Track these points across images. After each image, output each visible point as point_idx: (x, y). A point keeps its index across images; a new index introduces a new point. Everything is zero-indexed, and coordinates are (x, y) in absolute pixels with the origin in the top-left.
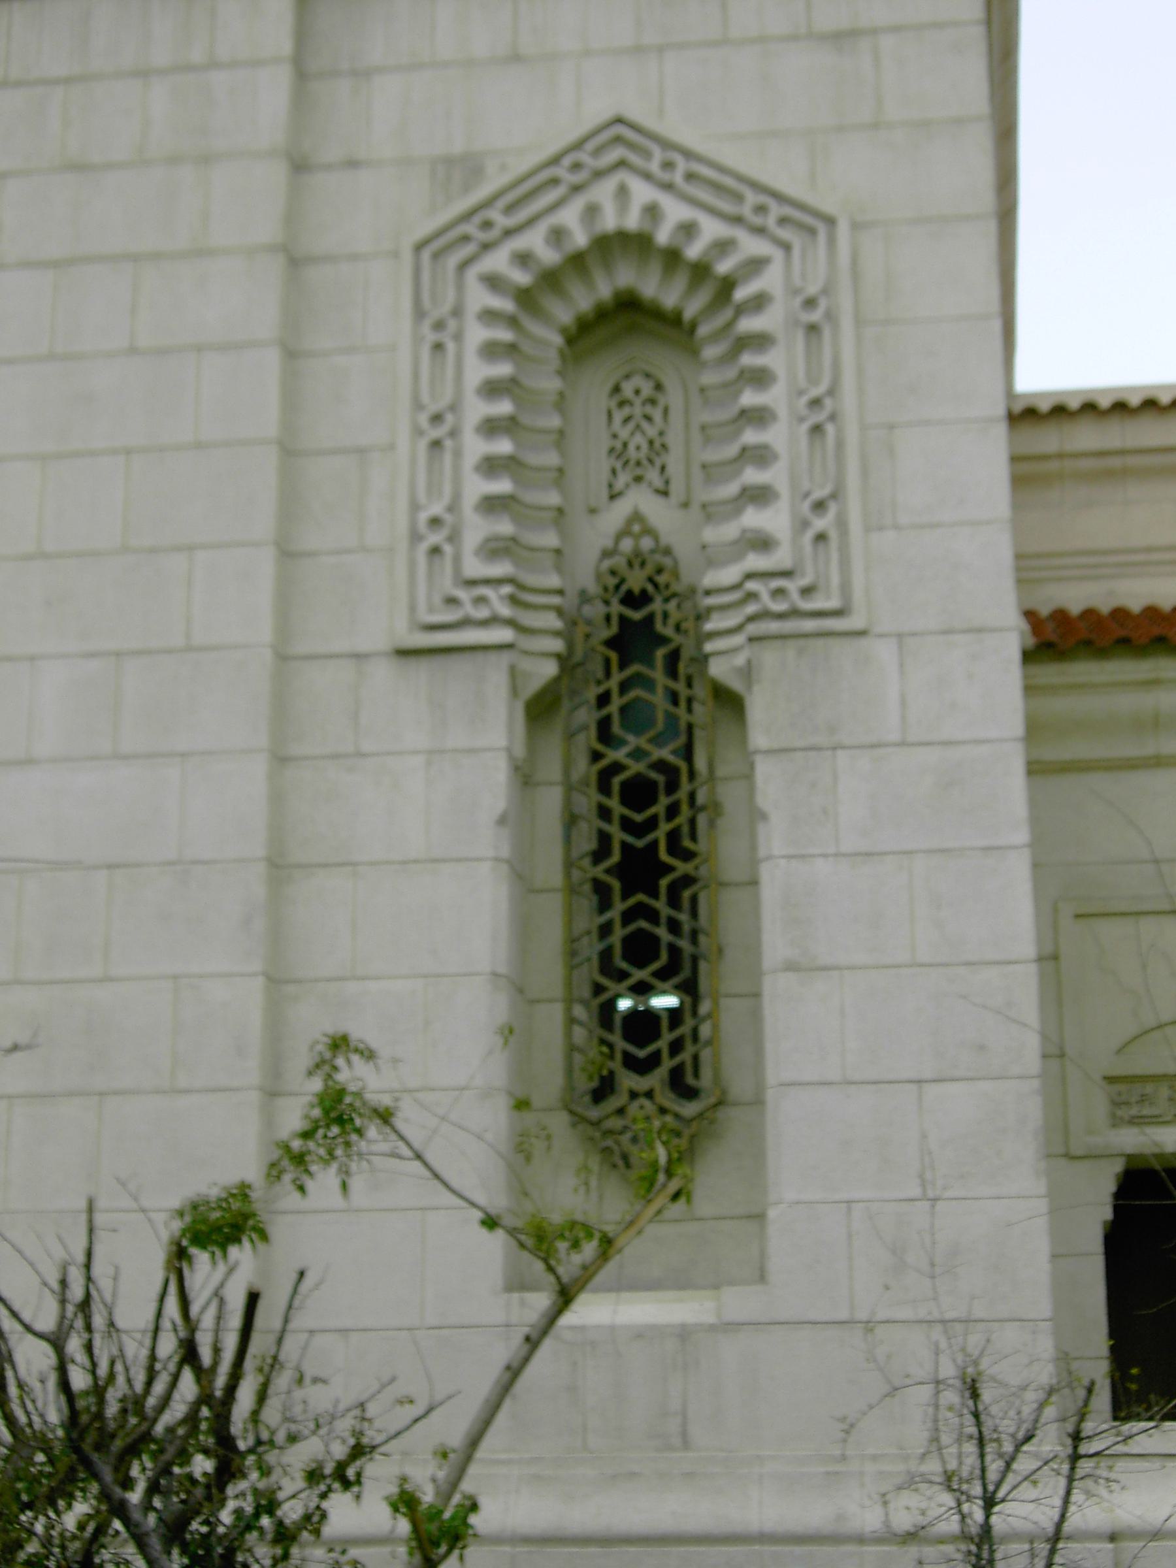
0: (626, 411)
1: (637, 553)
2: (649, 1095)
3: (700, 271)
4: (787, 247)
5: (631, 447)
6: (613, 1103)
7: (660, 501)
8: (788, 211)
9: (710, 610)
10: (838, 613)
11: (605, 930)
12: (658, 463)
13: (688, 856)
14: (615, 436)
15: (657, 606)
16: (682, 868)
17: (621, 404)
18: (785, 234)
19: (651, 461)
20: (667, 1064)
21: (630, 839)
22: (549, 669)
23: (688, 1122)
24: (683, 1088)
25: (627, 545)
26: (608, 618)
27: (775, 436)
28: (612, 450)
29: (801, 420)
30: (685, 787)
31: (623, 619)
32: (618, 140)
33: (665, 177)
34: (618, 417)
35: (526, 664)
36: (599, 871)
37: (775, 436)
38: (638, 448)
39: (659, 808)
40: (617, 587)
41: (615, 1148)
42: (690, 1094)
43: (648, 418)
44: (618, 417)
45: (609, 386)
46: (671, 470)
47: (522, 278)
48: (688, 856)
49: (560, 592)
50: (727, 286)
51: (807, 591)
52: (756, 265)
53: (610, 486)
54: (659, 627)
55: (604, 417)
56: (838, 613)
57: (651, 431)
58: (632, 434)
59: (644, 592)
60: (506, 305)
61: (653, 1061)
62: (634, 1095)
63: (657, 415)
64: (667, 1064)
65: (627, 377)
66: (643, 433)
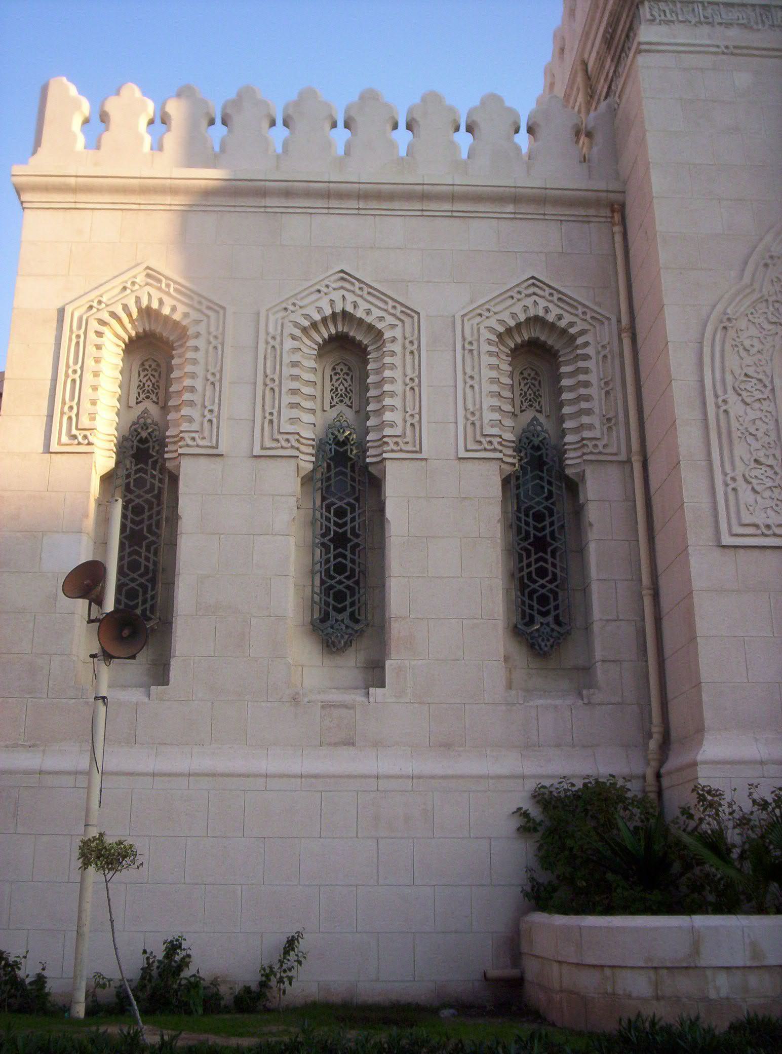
0: (338, 377)
1: (145, 424)
2: (548, 624)
3: (564, 331)
4: (403, 321)
5: (146, 386)
6: (329, 623)
7: (349, 409)
8: (404, 309)
9: (369, 447)
10: (615, 454)
11: (328, 561)
12: (538, 400)
13: (357, 536)
14: (140, 381)
15: (544, 451)
16: (525, 544)
17: (336, 374)
18: (403, 317)
19: (535, 400)
20: (349, 610)
21: (337, 529)
22: (310, 467)
23: (356, 631)
24: (354, 618)
25: (142, 421)
26: (330, 450)
27: (593, 391)
28: (521, 395)
29: (602, 389)
30: (156, 509)
31: (138, 448)
32: (533, 284)
33: (550, 298)
34: (335, 378)
35: (302, 464)
36: (556, 544)
37: (593, 391)
38: (149, 386)
39: (547, 523)
40: (529, 443)
41: (536, 643)
42: (357, 621)
43: (154, 376)
44: (142, 374)
45: (140, 363)
46: (543, 403)
47: (501, 329)
48: (357, 536)
49: (313, 440)
50: (573, 338)
51: (605, 446)
52: (583, 332)
53: (521, 407)
54: (151, 451)
55: (137, 375)
56: (615, 454)
57: (535, 390)
58: (147, 381)
59: (538, 445)
60: (494, 338)
61: (344, 609)
62: (542, 624)
63: (536, 383)
64: (349, 610)
65: (147, 360)
66: (151, 381)
